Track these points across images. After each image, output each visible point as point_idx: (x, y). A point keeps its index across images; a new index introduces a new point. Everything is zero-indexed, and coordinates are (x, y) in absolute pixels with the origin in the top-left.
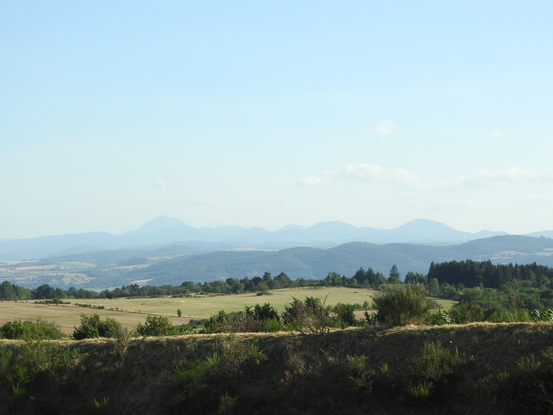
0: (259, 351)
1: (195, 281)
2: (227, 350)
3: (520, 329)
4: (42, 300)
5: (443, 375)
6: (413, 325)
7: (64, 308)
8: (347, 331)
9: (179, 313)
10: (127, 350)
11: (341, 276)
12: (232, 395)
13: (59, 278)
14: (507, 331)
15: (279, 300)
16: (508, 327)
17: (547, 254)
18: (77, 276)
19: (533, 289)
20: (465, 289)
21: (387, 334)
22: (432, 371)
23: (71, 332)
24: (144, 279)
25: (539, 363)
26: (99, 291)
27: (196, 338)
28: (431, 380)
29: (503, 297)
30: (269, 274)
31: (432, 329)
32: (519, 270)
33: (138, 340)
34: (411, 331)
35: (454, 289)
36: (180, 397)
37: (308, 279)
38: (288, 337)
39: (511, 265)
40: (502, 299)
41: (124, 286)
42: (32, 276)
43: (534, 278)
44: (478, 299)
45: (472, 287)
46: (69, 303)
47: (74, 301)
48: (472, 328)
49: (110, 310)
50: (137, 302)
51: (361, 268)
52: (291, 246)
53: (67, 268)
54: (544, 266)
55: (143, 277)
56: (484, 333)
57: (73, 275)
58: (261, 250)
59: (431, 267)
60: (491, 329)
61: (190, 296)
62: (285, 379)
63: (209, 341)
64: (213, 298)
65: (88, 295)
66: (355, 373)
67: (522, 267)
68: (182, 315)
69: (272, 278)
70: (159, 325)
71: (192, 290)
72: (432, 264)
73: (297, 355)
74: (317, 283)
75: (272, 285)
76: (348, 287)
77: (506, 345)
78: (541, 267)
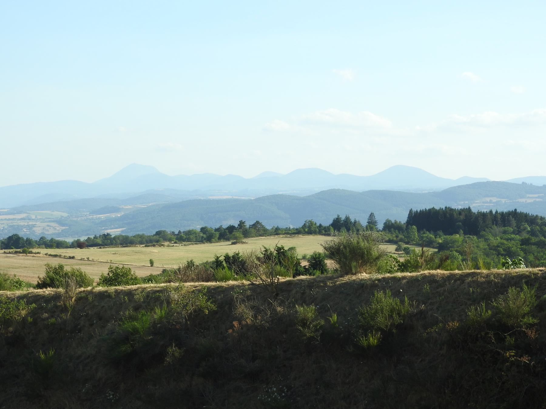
0: (207, 301)
1: (169, 230)
2: (175, 300)
3: (473, 278)
4: (11, 250)
5: (392, 325)
6: (364, 274)
7: (34, 258)
8: (298, 280)
9: (152, 263)
10: (75, 300)
11: (318, 225)
12: (179, 345)
13: (30, 227)
14: (459, 279)
15: (251, 248)
16: (461, 275)
17: (529, 201)
18: (48, 226)
19: (513, 236)
20: (444, 237)
21: (338, 283)
22: (381, 320)
23: (97, 279)
24: (117, 228)
25: (490, 312)
26: (70, 240)
27: (145, 288)
28: (379, 329)
29: (483, 245)
30: (244, 223)
31: (384, 278)
32: (499, 217)
33: (87, 291)
34: (362, 280)
35: (432, 236)
36: (125, 348)
37: (285, 227)
38: (238, 286)
39: (491, 212)
40: (482, 247)
41: (96, 236)
42: (3, 226)
43: (515, 224)
44: (458, 247)
45: (451, 234)
46: (38, 253)
47: (43, 251)
48: (424, 277)
49: (81, 260)
50: (108, 251)
51: (338, 216)
52: (268, 193)
53: (39, 217)
54: (525, 212)
55: (117, 226)
56: (435, 281)
57: (44, 224)
58: (237, 197)
59: (409, 214)
60: (443, 278)
61: (162, 245)
62: (233, 330)
63: (158, 291)
64: (187, 247)
65: (59, 245)
66: (304, 323)
67: (502, 214)
68: (155, 265)
69: (248, 226)
70: (122, 276)
71: (165, 240)
72: (411, 211)
73: (245, 305)
74: (293, 232)
75: (247, 234)
76: (325, 235)
77: (458, 293)
78: (521, 214)
